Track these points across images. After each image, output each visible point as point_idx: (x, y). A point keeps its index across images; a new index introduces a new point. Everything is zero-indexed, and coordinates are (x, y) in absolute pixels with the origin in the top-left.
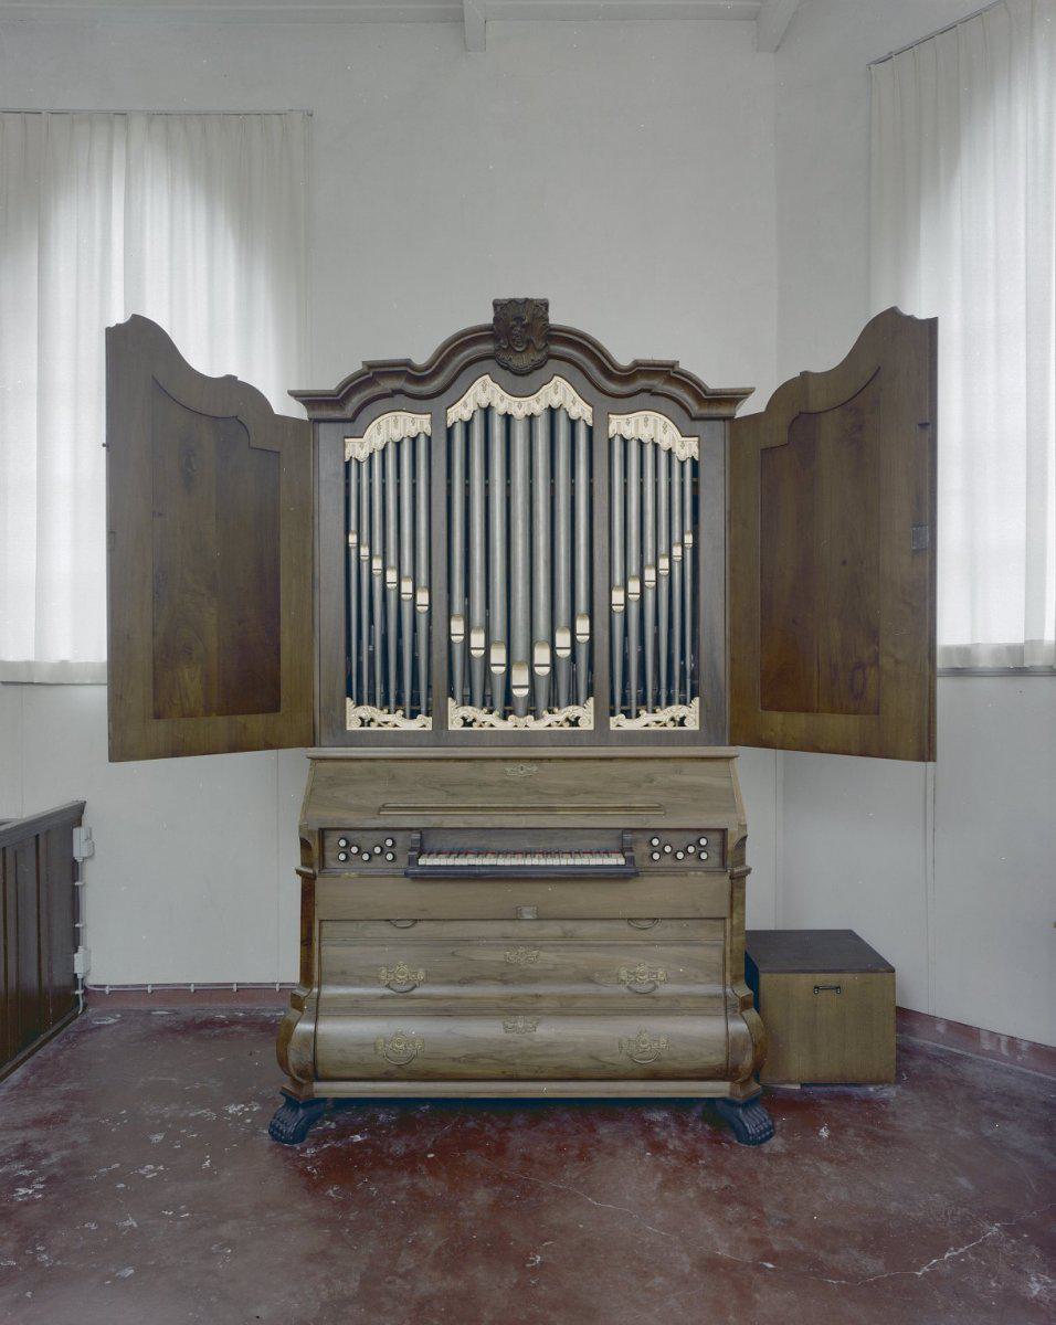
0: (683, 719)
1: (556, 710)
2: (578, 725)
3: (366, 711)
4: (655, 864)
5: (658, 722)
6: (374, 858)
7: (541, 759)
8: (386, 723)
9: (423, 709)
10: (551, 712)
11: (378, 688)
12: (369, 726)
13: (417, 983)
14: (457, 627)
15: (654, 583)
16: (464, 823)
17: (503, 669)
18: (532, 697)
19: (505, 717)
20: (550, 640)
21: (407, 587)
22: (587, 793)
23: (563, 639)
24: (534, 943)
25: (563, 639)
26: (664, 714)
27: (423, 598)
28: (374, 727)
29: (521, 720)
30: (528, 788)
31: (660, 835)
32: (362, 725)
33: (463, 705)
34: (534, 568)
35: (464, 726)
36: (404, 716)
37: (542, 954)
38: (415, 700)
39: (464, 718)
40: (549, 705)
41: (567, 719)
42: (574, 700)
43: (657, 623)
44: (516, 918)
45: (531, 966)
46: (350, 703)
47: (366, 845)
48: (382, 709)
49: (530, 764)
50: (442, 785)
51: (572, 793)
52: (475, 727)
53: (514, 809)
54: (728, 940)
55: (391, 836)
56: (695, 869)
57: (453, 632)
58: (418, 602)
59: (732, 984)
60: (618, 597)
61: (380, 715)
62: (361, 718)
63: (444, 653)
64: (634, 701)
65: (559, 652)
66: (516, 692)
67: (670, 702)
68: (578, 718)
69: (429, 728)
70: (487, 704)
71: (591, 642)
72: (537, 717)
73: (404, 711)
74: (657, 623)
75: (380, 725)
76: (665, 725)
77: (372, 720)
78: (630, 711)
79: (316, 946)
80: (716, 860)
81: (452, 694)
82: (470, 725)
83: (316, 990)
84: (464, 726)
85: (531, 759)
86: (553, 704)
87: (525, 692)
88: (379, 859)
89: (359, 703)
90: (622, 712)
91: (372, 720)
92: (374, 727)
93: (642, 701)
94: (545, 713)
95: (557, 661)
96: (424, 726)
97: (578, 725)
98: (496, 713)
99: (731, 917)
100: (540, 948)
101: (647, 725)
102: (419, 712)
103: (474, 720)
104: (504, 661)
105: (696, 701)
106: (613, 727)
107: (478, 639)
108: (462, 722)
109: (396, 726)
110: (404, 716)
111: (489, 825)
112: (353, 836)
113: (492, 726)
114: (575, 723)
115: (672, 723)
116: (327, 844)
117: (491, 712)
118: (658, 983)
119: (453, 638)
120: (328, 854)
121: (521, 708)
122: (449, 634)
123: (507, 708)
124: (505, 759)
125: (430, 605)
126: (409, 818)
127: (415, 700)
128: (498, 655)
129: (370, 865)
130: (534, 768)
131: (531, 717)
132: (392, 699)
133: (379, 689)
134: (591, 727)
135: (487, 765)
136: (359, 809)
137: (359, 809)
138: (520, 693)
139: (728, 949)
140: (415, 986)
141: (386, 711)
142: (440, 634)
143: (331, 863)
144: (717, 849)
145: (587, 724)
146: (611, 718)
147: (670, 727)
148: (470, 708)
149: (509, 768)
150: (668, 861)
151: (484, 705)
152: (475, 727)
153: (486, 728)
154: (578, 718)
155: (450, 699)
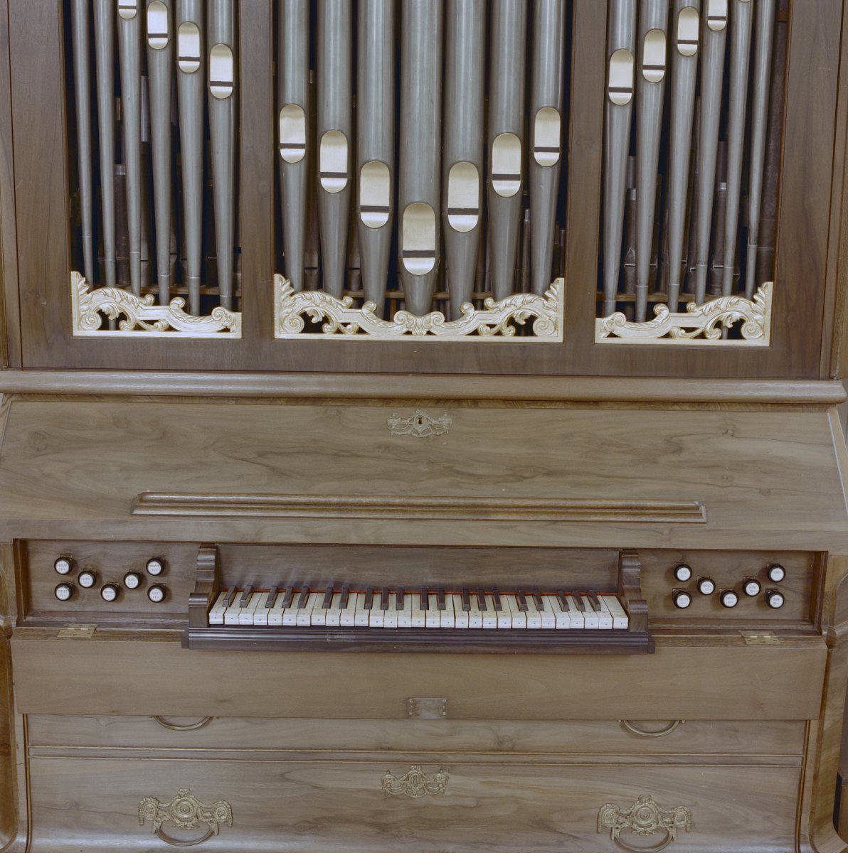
0: (739, 324)
1: (489, 302)
2: (531, 333)
3: (111, 299)
4: (682, 613)
5: (689, 330)
6: (127, 595)
7: (458, 401)
8: (151, 322)
9: (225, 295)
10: (479, 305)
11: (134, 253)
12: (117, 328)
13: (214, 827)
14: (293, 129)
15: (695, 47)
16: (307, 534)
17: (343, 183)
18: (441, 277)
19: (387, 315)
20: (480, 163)
21: (189, 44)
22: (548, 474)
23: (506, 158)
24: (437, 758)
25: (506, 158)
26: (703, 315)
27: (222, 68)
28: (126, 331)
29: (419, 320)
30: (431, 463)
31: (692, 559)
32: (105, 326)
33: (305, 287)
34: (451, 61)
35: (304, 331)
36: (187, 309)
37: (455, 780)
38: (209, 274)
39: (305, 316)
40: (475, 290)
41: (511, 321)
42: (523, 283)
43: (633, 148)
44: (409, 711)
45: (435, 802)
46: (77, 282)
47: (110, 570)
48: (143, 295)
49: (437, 411)
50: (262, 455)
51: (518, 473)
52: (328, 334)
53: (404, 508)
54: (811, 756)
55: (158, 554)
56: (759, 625)
57: (283, 140)
58: (181, 53)
59: (812, 836)
60: (621, 73)
61: (141, 309)
62: (101, 313)
63: (267, 185)
64: (643, 287)
65: (454, 221)
66: (410, 265)
67: (712, 290)
68: (532, 319)
69: (236, 334)
70: (353, 286)
71: (564, 166)
72: (450, 317)
73: (186, 297)
74: (633, 148)
75: (138, 328)
76: (702, 336)
77: (123, 317)
78: (633, 305)
79: (20, 758)
80: (797, 607)
81: (281, 267)
82: (317, 328)
83: (21, 839)
84: (304, 331)
85: (440, 401)
86: (481, 292)
87: (428, 265)
88: (136, 595)
89: (98, 282)
90: (620, 307)
91: (123, 317)
92: (126, 331)
93: (657, 282)
94: (468, 307)
95: (493, 202)
96: (226, 330)
97: (531, 333)
98: (370, 306)
99: (821, 717)
100: (449, 767)
101: (667, 336)
102: (216, 301)
103: (326, 320)
104: (385, 201)
105: (766, 292)
106: (601, 338)
107: (334, 156)
108: (301, 323)
109: (170, 329)
110: (187, 309)
111: (354, 539)
112: (86, 554)
113: (361, 331)
114: (526, 328)
115: (718, 332)
116: (33, 566)
117: (359, 303)
118: (672, 832)
119: (285, 153)
120: (38, 587)
121: (419, 295)
122: (277, 145)
123: (393, 295)
124: (386, 400)
125: (237, 84)
126: (193, 521)
127: (209, 274)
128: (374, 189)
129: (117, 607)
130: (445, 419)
131: (437, 316)
132: (164, 275)
133: (137, 253)
134: (558, 337)
135: (352, 412)
136: (91, 503)
137: (91, 503)
138: (419, 267)
139: (810, 773)
140: (210, 835)
141: (150, 298)
142: (254, 143)
143: (41, 601)
144: (800, 586)
145: (550, 331)
146: (598, 320)
147: (715, 339)
148: (317, 295)
149: (396, 419)
150: (704, 609)
151: (346, 287)
152: (328, 334)
153: (349, 335)
154: (532, 319)
155: (277, 276)
